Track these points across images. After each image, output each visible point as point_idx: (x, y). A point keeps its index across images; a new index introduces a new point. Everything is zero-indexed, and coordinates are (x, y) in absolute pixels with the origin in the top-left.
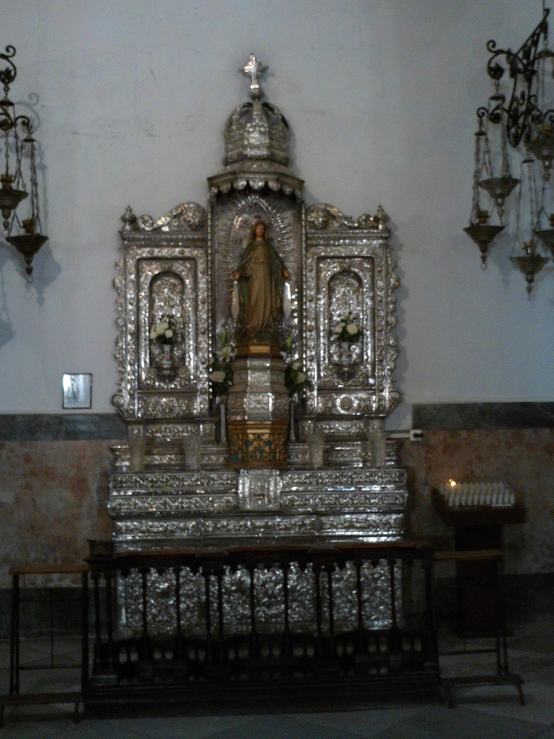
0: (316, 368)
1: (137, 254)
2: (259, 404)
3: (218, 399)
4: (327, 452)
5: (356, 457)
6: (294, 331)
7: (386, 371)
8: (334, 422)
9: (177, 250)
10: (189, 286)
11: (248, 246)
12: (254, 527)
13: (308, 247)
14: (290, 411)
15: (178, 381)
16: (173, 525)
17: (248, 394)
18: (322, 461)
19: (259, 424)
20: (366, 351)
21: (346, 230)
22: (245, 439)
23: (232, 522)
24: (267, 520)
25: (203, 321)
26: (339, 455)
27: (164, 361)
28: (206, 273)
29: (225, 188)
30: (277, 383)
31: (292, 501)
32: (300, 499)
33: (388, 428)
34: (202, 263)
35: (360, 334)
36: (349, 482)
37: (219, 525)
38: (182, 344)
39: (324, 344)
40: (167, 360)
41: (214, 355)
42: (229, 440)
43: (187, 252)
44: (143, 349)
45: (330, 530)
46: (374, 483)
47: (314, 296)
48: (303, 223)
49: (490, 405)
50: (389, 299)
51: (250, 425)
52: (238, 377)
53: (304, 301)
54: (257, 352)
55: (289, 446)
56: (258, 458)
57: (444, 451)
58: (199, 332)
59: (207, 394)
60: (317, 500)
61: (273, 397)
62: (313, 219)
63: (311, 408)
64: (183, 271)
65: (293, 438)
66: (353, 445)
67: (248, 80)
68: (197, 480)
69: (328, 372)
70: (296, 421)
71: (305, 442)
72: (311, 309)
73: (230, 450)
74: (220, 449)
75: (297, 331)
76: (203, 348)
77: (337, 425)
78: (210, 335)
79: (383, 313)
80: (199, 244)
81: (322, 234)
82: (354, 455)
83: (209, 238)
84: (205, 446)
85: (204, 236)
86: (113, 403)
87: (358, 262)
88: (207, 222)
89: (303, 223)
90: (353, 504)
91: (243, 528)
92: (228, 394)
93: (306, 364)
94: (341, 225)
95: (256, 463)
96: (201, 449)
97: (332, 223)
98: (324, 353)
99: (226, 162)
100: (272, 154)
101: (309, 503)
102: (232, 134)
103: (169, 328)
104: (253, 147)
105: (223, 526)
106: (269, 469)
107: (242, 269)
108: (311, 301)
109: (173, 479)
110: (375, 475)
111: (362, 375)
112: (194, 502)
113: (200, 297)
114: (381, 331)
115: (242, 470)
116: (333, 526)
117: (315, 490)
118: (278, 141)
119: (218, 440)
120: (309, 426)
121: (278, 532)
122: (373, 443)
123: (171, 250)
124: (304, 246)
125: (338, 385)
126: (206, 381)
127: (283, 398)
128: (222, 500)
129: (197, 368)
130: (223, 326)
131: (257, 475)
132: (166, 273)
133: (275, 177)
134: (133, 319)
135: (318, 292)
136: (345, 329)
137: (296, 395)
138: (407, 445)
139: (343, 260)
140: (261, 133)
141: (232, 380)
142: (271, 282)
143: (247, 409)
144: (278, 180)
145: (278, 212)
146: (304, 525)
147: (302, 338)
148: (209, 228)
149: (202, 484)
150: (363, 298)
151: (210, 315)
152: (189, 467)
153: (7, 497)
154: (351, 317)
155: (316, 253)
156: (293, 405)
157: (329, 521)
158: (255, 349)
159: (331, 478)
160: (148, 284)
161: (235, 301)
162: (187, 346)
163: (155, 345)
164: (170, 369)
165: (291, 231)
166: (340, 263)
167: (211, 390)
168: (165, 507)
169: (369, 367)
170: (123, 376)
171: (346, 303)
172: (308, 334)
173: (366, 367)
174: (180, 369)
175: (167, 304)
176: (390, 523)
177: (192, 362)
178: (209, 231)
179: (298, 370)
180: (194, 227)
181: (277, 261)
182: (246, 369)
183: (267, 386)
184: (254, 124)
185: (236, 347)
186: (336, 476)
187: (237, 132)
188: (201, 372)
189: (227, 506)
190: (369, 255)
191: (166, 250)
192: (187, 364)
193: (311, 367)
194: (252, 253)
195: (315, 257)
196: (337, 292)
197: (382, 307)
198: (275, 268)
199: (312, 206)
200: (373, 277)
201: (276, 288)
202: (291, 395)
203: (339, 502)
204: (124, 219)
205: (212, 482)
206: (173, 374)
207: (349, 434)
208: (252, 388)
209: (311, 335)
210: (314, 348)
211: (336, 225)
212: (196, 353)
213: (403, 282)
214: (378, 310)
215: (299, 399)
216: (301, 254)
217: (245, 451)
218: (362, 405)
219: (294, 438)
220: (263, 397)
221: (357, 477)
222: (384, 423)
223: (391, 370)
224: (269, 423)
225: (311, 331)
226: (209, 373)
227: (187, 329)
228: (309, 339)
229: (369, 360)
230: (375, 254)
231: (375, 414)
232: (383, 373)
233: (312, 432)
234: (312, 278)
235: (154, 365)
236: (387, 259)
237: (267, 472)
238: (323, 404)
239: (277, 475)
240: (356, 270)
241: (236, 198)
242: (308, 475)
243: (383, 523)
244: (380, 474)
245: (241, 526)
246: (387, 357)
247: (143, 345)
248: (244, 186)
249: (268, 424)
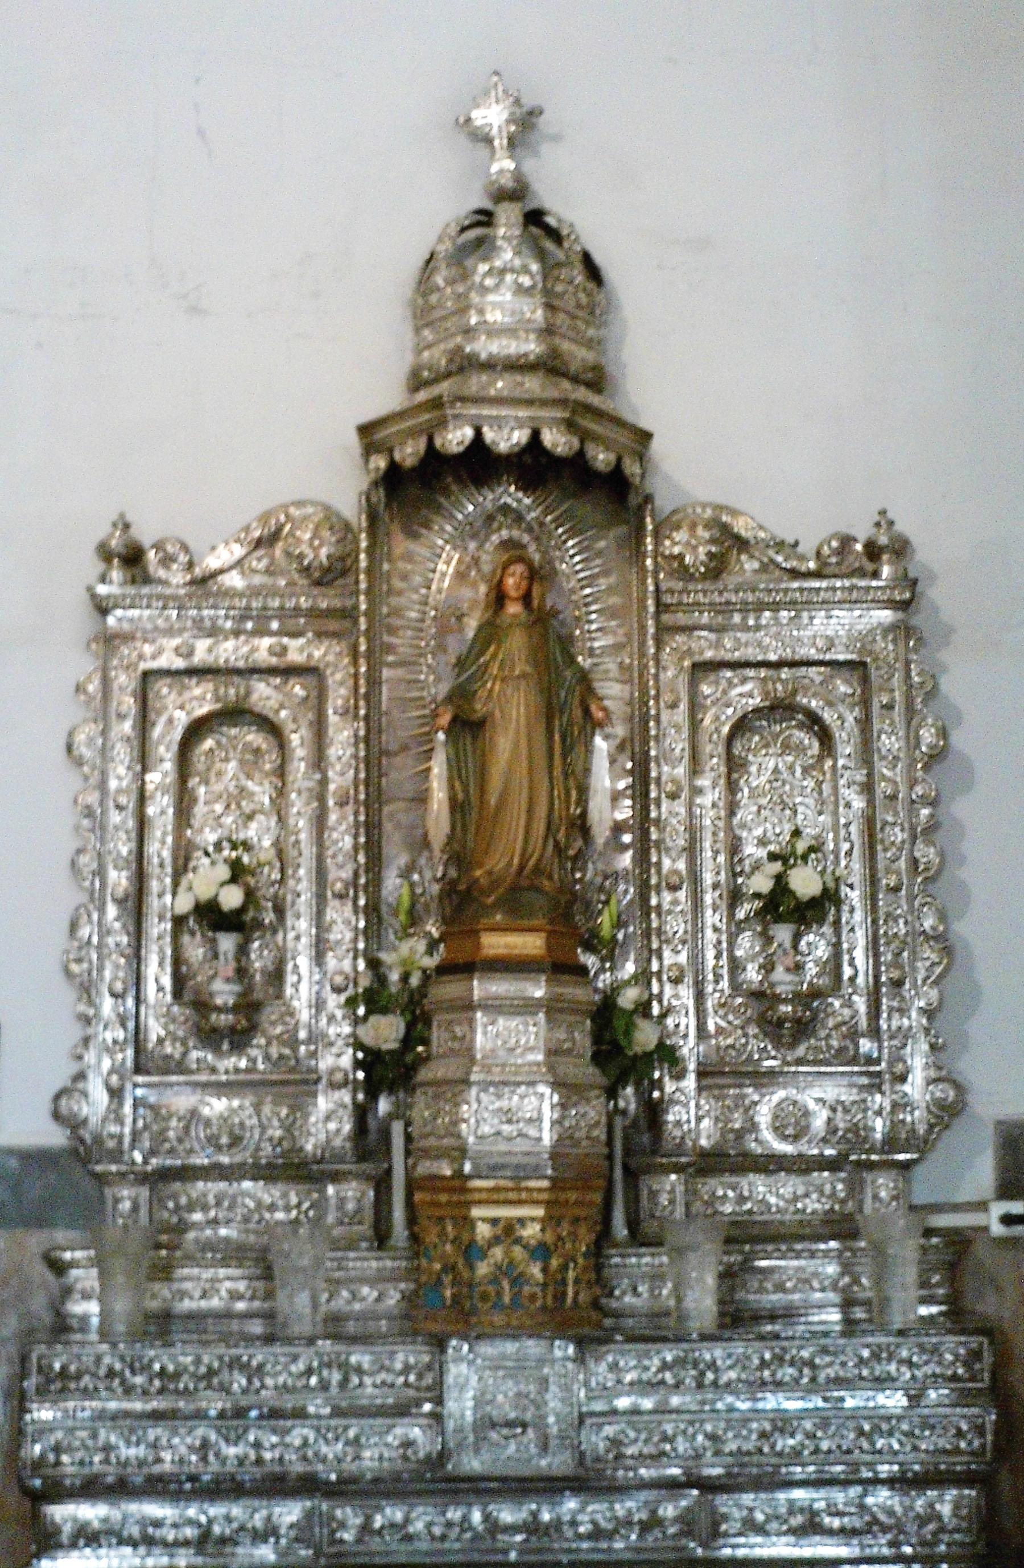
0: (691, 1004)
1: (141, 657)
2: (509, 1121)
3: (384, 1105)
4: (728, 1276)
5: (823, 1290)
6: (622, 887)
7: (914, 1014)
8: (751, 1176)
9: (266, 642)
10: (300, 752)
11: (480, 628)
12: (493, 1527)
13: (663, 632)
14: (610, 1142)
15: (258, 1046)
16: (228, 1519)
17: (474, 1091)
18: (715, 1309)
19: (507, 1190)
20: (850, 951)
21: (781, 581)
22: (466, 1237)
23: (421, 1509)
24: (534, 1506)
25: (340, 858)
26: (769, 1286)
27: (218, 985)
28: (351, 715)
29: (409, 453)
30: (569, 1052)
31: (615, 1442)
32: (643, 1436)
33: (920, 1197)
34: (342, 683)
36: (805, 1380)
37: (378, 1521)
38: (275, 932)
39: (716, 929)
40: (228, 980)
41: (374, 964)
42: (415, 1238)
43: (297, 650)
44: (154, 948)
45: (742, 1540)
46: (882, 1382)
47: (685, 783)
48: (649, 562)
50: (919, 790)
51: (480, 1190)
52: (446, 1035)
53: (653, 795)
54: (502, 951)
55: (609, 1257)
56: (507, 1299)
58: (329, 894)
59: (350, 1087)
60: (700, 1438)
61: (556, 1098)
62: (676, 550)
63: (678, 1133)
64: (282, 706)
65: (620, 1230)
66: (813, 1255)
67: (483, 151)
68: (309, 1372)
69: (731, 1017)
70: (631, 1175)
71: (660, 1244)
72: (674, 821)
73: (418, 1268)
74: (389, 1263)
75: (632, 890)
76: (338, 942)
77: (761, 1189)
78: (362, 902)
79: (899, 835)
80: (333, 625)
81: (705, 592)
82: (816, 1284)
83: (363, 607)
84: (339, 1254)
85: (349, 603)
86: (56, 1116)
87: (818, 679)
88: (357, 559)
89: (649, 562)
90: (816, 1451)
91: (457, 1529)
92: (414, 1089)
93: (661, 992)
94: (764, 568)
95: (498, 1319)
96: (329, 1264)
97: (739, 560)
98: (718, 957)
99: (416, 382)
100: (554, 353)
101: (674, 1449)
102: (434, 298)
103: (234, 879)
104: (494, 332)
105: (393, 1525)
106: (539, 1336)
108: (673, 796)
109: (231, 1367)
110: (889, 1359)
111: (837, 1027)
112: (297, 1442)
113: (332, 787)
114: (896, 889)
115: (454, 1342)
116: (751, 1526)
117: (694, 1407)
118: (574, 317)
119: (381, 1237)
120: (672, 1191)
121: (574, 1545)
122: (878, 1250)
123: (247, 641)
124: (651, 630)
125: (760, 1059)
126: (347, 1045)
127: (588, 1100)
128: (390, 1439)
129: (319, 1005)
130: (405, 874)
131: (504, 1357)
133: (559, 414)
134: (124, 851)
135: (695, 769)
136: (781, 883)
137: (629, 1090)
138: (981, 1250)
139: (771, 672)
140: (520, 290)
141: (426, 1042)
142: (550, 737)
143: (471, 1140)
144: (570, 425)
145: (572, 533)
146: (652, 1523)
147: (646, 910)
148: (362, 577)
149: (324, 1386)
150: (835, 789)
151: (362, 840)
152: (285, 1325)
154: (801, 846)
155: (689, 652)
156: (619, 1122)
157: (740, 1507)
159: (744, 1368)
160: (175, 747)
161: (439, 794)
162: (291, 935)
163: (193, 934)
164: (236, 1009)
165: (610, 590)
166: (764, 680)
167: (361, 1075)
168: (204, 1459)
169: (861, 1003)
170: (90, 1031)
171: (784, 806)
172: (667, 897)
173: (849, 1004)
174: (269, 1009)
175: (233, 806)
176: (939, 1517)
177: (304, 987)
178: (363, 586)
179: (634, 1011)
180: (317, 574)
181: (568, 674)
182: (469, 1006)
183: (538, 1064)
184: (498, 263)
185: (441, 939)
186: (762, 1359)
187: (449, 290)
188: (331, 1018)
189: (405, 1458)
190: (853, 657)
191: (230, 644)
192: (289, 991)
193: (674, 1003)
194: (492, 649)
195: (687, 663)
196: (753, 769)
197: (896, 814)
198: (563, 694)
199: (674, 512)
200: (865, 724)
201: (564, 756)
202: (612, 1093)
203: (773, 1447)
204: (105, 553)
205: (355, 1380)
206: (244, 1022)
207: (798, 1217)
208: (487, 1069)
209: (675, 902)
210: (684, 942)
211: (750, 565)
212: (319, 958)
213: (958, 739)
214: (885, 823)
215: (638, 1103)
216: (642, 654)
217: (466, 1275)
218: (841, 1125)
219: (625, 1232)
220: (522, 1097)
221: (830, 1364)
222: (907, 1181)
223: (929, 1013)
224: (545, 1184)
225: (674, 888)
226: (357, 1021)
227: (291, 883)
228: (669, 912)
229: (860, 980)
230: (870, 653)
231: (882, 1152)
232: (906, 1022)
233: (679, 1212)
234: (678, 728)
235: (187, 996)
236: (908, 671)
237: (533, 1347)
238: (717, 1119)
239: (567, 1358)
240: (813, 703)
241: (446, 492)
242: (669, 1358)
243: (918, 1516)
244: (905, 1354)
245: (449, 1524)
246: (914, 970)
247: (155, 932)
248: (467, 443)
249: (540, 1190)
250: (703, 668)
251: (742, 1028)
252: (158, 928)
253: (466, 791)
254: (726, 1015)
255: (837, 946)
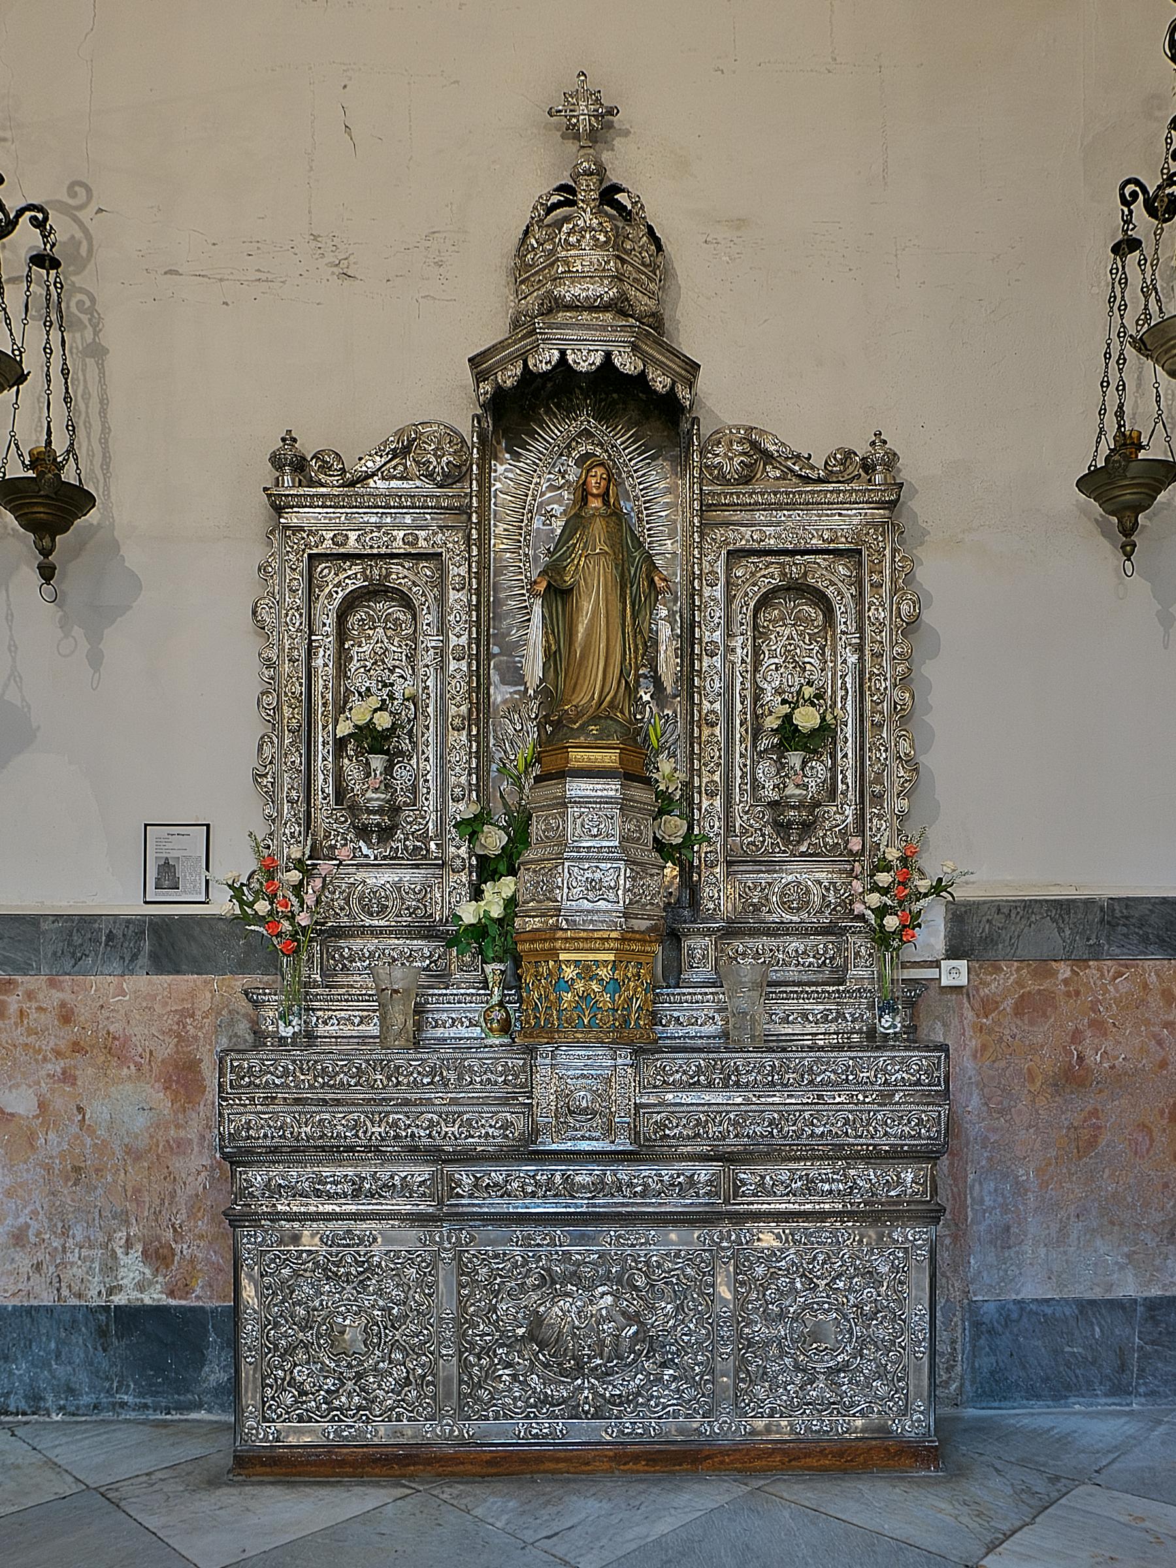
35: (825, 732)
49: (1128, 902)
57: (1018, 1011)
99: (516, 324)
107: (553, 570)
132: (376, 591)
153: (21, 1103)
158: (579, 757)
172: (706, 731)
182: (563, 803)
200: (859, 598)
201: (634, 617)
204: (277, 462)
250: (737, 554)
251: (761, 830)
252: (322, 751)
253: (558, 642)
254: (749, 820)
255: (833, 769)
